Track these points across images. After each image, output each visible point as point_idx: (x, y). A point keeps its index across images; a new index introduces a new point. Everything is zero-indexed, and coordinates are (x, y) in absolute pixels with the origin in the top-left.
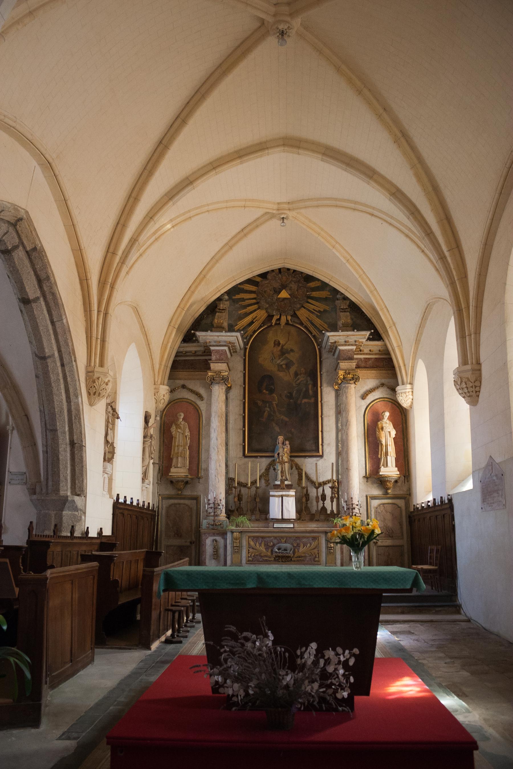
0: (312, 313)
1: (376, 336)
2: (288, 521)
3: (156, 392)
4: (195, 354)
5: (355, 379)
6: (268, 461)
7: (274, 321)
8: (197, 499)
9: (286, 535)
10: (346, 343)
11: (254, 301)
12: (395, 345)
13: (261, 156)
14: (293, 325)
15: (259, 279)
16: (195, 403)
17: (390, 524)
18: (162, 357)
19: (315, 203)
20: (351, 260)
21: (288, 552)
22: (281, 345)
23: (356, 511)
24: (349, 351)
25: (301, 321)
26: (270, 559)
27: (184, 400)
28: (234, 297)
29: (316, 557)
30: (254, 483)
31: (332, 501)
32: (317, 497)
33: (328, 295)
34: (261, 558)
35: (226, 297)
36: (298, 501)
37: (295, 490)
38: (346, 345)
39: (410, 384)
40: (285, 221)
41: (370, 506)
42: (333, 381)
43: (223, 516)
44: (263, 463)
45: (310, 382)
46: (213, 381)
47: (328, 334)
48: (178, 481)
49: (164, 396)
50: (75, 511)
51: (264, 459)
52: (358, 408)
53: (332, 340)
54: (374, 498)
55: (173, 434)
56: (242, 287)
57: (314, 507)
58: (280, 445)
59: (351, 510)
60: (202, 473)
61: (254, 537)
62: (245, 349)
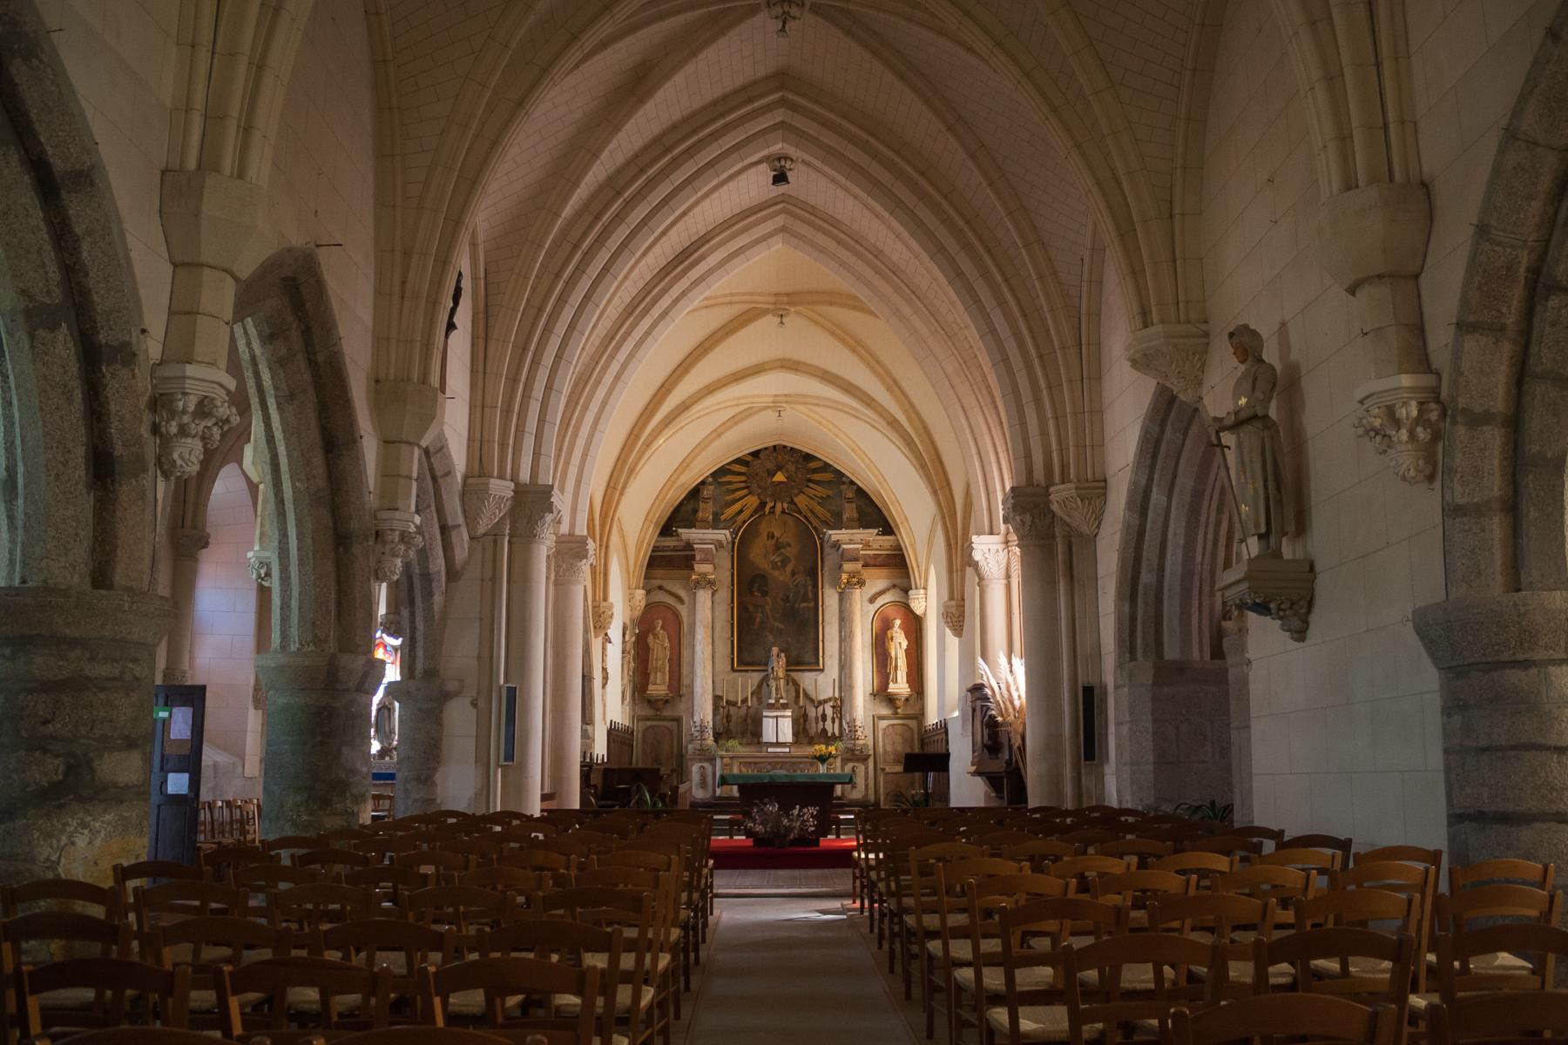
0: (812, 499)
2: (783, 745)
3: (631, 598)
4: (675, 549)
5: (861, 583)
6: (762, 674)
7: (767, 509)
8: (678, 720)
10: (851, 542)
11: (743, 485)
12: (907, 544)
15: (750, 458)
17: (900, 748)
18: (637, 556)
23: (859, 733)
30: (745, 701)
31: (833, 722)
32: (817, 718)
35: (710, 479)
36: (795, 722)
42: (835, 583)
43: (710, 740)
44: (755, 678)
45: (809, 582)
46: (697, 584)
47: (830, 532)
48: (657, 700)
51: (755, 674)
53: (834, 538)
54: (882, 718)
57: (814, 729)
58: (775, 657)
60: (684, 691)
61: (746, 763)
62: (733, 543)
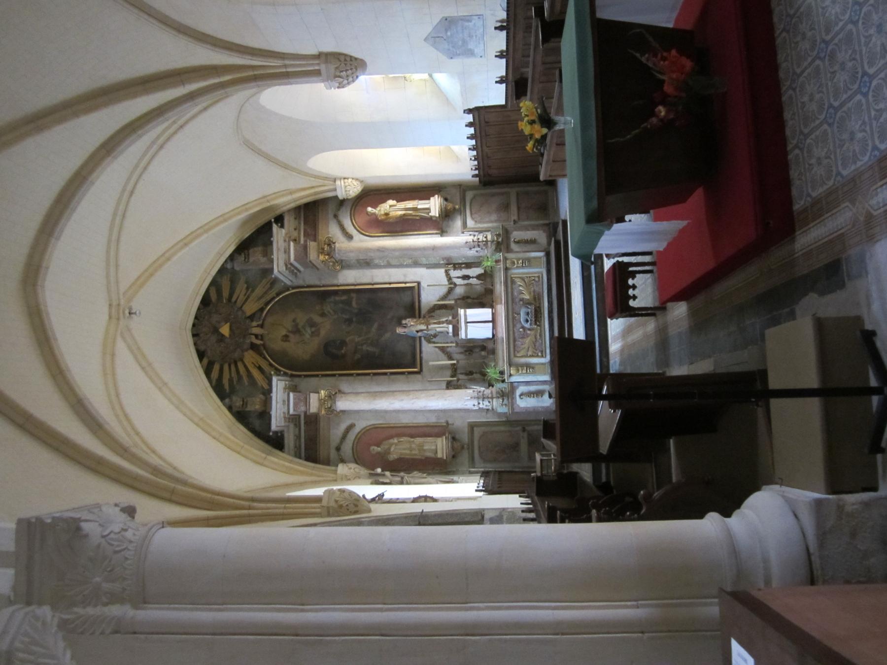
1: (279, 219)
5: (330, 243)
8: (472, 426)
9: (510, 313)
10: (287, 251)
12: (289, 198)
13: (48, 314)
14: (264, 320)
15: (205, 361)
16: (359, 433)
19: (112, 269)
20: (185, 241)
21: (529, 310)
22: (288, 334)
24: (295, 250)
26: (539, 331)
27: (355, 448)
28: (228, 391)
29: (534, 280)
34: (538, 341)
35: (227, 400)
37: (459, 309)
39: (335, 181)
40: (134, 311)
41: (474, 228)
45: (332, 299)
46: (331, 410)
48: (453, 448)
50: (503, 518)
52: (361, 241)
55: (396, 458)
56: (214, 382)
58: (406, 330)
59: (479, 243)
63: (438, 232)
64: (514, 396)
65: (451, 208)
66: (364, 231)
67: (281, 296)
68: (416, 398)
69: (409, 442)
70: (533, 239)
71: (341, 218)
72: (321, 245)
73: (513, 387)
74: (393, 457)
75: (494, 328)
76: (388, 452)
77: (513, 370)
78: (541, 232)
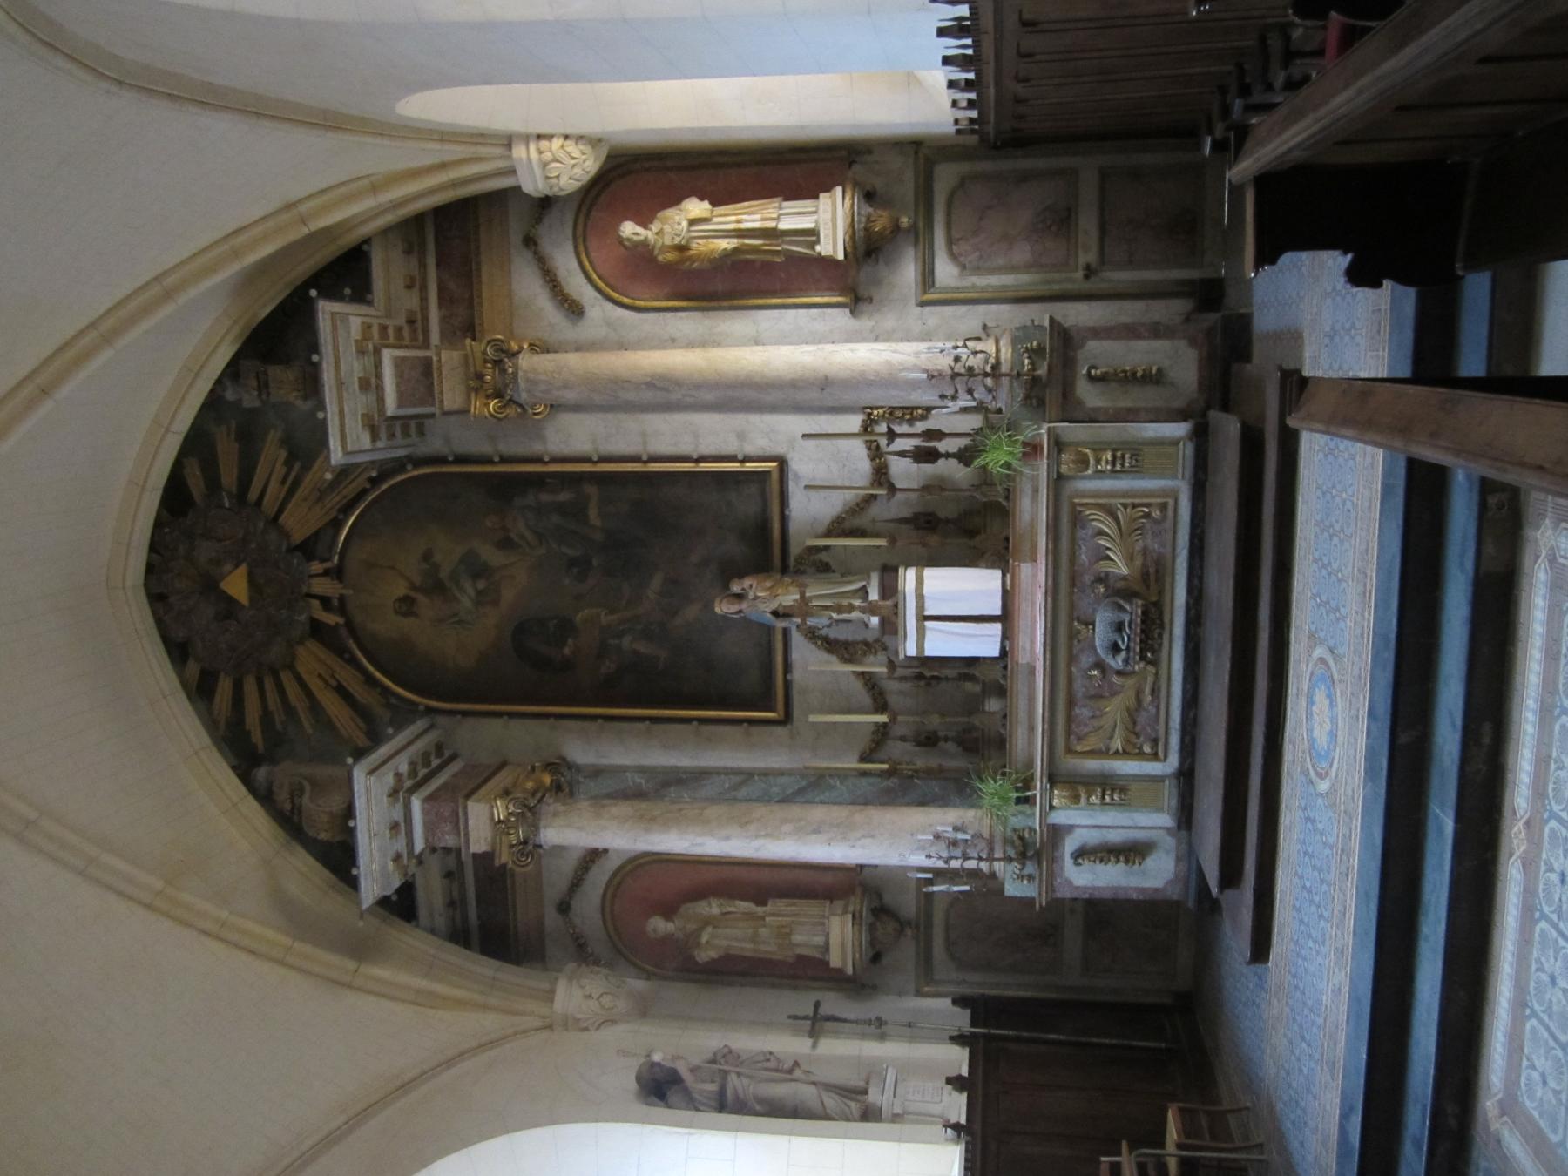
0: (296, 484)
10: (373, 384)
11: (269, 684)
12: (368, 203)
14: (342, 555)
21: (1127, 618)
22: (412, 594)
25: (327, 524)
26: (1150, 679)
29: (1147, 516)
33: (229, 435)
35: (261, 773)
38: (380, 389)
39: (509, 146)
41: (957, 289)
45: (530, 499)
48: (873, 942)
49: (590, 996)
54: (927, 278)
61: (1069, 733)
62: (430, 711)
63: (840, 299)
64: (1056, 854)
65: (884, 228)
66: (618, 293)
67: (384, 487)
68: (767, 835)
69: (750, 916)
70: (1154, 370)
71: (546, 246)
72: (475, 365)
73: (1056, 833)
74: (704, 956)
75: (1006, 636)
76: (692, 939)
77: (1060, 797)
78: (1182, 344)
